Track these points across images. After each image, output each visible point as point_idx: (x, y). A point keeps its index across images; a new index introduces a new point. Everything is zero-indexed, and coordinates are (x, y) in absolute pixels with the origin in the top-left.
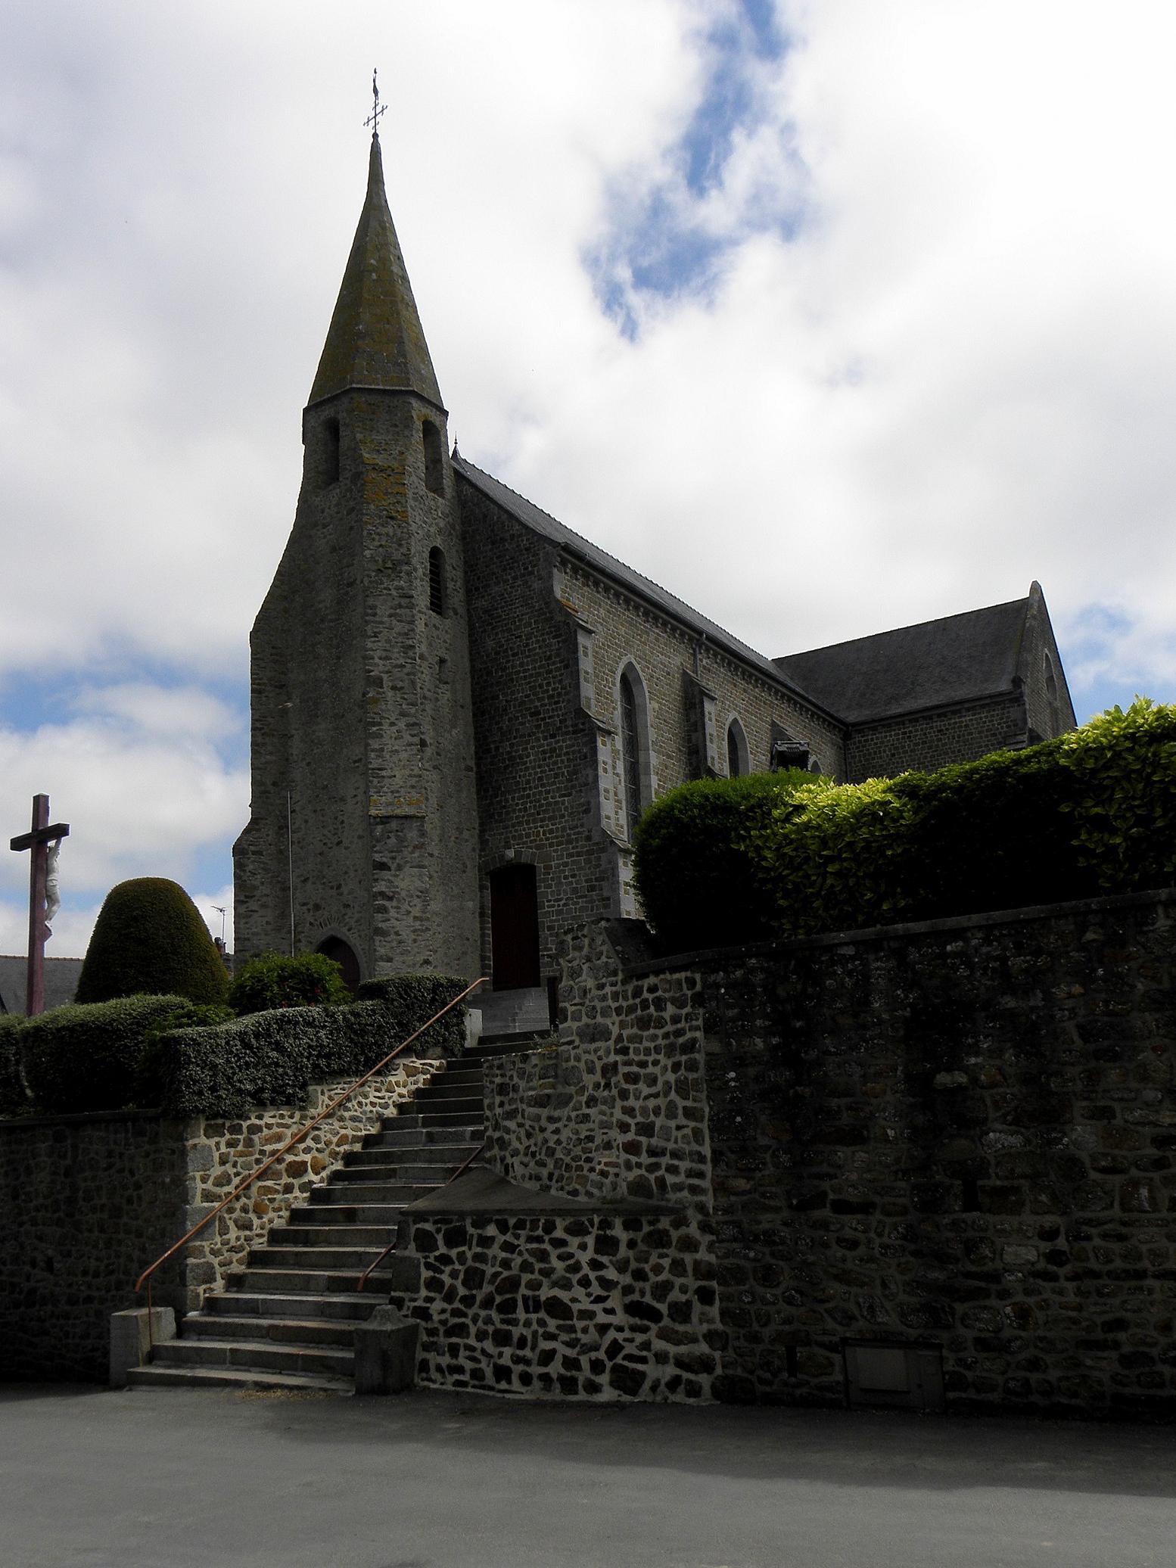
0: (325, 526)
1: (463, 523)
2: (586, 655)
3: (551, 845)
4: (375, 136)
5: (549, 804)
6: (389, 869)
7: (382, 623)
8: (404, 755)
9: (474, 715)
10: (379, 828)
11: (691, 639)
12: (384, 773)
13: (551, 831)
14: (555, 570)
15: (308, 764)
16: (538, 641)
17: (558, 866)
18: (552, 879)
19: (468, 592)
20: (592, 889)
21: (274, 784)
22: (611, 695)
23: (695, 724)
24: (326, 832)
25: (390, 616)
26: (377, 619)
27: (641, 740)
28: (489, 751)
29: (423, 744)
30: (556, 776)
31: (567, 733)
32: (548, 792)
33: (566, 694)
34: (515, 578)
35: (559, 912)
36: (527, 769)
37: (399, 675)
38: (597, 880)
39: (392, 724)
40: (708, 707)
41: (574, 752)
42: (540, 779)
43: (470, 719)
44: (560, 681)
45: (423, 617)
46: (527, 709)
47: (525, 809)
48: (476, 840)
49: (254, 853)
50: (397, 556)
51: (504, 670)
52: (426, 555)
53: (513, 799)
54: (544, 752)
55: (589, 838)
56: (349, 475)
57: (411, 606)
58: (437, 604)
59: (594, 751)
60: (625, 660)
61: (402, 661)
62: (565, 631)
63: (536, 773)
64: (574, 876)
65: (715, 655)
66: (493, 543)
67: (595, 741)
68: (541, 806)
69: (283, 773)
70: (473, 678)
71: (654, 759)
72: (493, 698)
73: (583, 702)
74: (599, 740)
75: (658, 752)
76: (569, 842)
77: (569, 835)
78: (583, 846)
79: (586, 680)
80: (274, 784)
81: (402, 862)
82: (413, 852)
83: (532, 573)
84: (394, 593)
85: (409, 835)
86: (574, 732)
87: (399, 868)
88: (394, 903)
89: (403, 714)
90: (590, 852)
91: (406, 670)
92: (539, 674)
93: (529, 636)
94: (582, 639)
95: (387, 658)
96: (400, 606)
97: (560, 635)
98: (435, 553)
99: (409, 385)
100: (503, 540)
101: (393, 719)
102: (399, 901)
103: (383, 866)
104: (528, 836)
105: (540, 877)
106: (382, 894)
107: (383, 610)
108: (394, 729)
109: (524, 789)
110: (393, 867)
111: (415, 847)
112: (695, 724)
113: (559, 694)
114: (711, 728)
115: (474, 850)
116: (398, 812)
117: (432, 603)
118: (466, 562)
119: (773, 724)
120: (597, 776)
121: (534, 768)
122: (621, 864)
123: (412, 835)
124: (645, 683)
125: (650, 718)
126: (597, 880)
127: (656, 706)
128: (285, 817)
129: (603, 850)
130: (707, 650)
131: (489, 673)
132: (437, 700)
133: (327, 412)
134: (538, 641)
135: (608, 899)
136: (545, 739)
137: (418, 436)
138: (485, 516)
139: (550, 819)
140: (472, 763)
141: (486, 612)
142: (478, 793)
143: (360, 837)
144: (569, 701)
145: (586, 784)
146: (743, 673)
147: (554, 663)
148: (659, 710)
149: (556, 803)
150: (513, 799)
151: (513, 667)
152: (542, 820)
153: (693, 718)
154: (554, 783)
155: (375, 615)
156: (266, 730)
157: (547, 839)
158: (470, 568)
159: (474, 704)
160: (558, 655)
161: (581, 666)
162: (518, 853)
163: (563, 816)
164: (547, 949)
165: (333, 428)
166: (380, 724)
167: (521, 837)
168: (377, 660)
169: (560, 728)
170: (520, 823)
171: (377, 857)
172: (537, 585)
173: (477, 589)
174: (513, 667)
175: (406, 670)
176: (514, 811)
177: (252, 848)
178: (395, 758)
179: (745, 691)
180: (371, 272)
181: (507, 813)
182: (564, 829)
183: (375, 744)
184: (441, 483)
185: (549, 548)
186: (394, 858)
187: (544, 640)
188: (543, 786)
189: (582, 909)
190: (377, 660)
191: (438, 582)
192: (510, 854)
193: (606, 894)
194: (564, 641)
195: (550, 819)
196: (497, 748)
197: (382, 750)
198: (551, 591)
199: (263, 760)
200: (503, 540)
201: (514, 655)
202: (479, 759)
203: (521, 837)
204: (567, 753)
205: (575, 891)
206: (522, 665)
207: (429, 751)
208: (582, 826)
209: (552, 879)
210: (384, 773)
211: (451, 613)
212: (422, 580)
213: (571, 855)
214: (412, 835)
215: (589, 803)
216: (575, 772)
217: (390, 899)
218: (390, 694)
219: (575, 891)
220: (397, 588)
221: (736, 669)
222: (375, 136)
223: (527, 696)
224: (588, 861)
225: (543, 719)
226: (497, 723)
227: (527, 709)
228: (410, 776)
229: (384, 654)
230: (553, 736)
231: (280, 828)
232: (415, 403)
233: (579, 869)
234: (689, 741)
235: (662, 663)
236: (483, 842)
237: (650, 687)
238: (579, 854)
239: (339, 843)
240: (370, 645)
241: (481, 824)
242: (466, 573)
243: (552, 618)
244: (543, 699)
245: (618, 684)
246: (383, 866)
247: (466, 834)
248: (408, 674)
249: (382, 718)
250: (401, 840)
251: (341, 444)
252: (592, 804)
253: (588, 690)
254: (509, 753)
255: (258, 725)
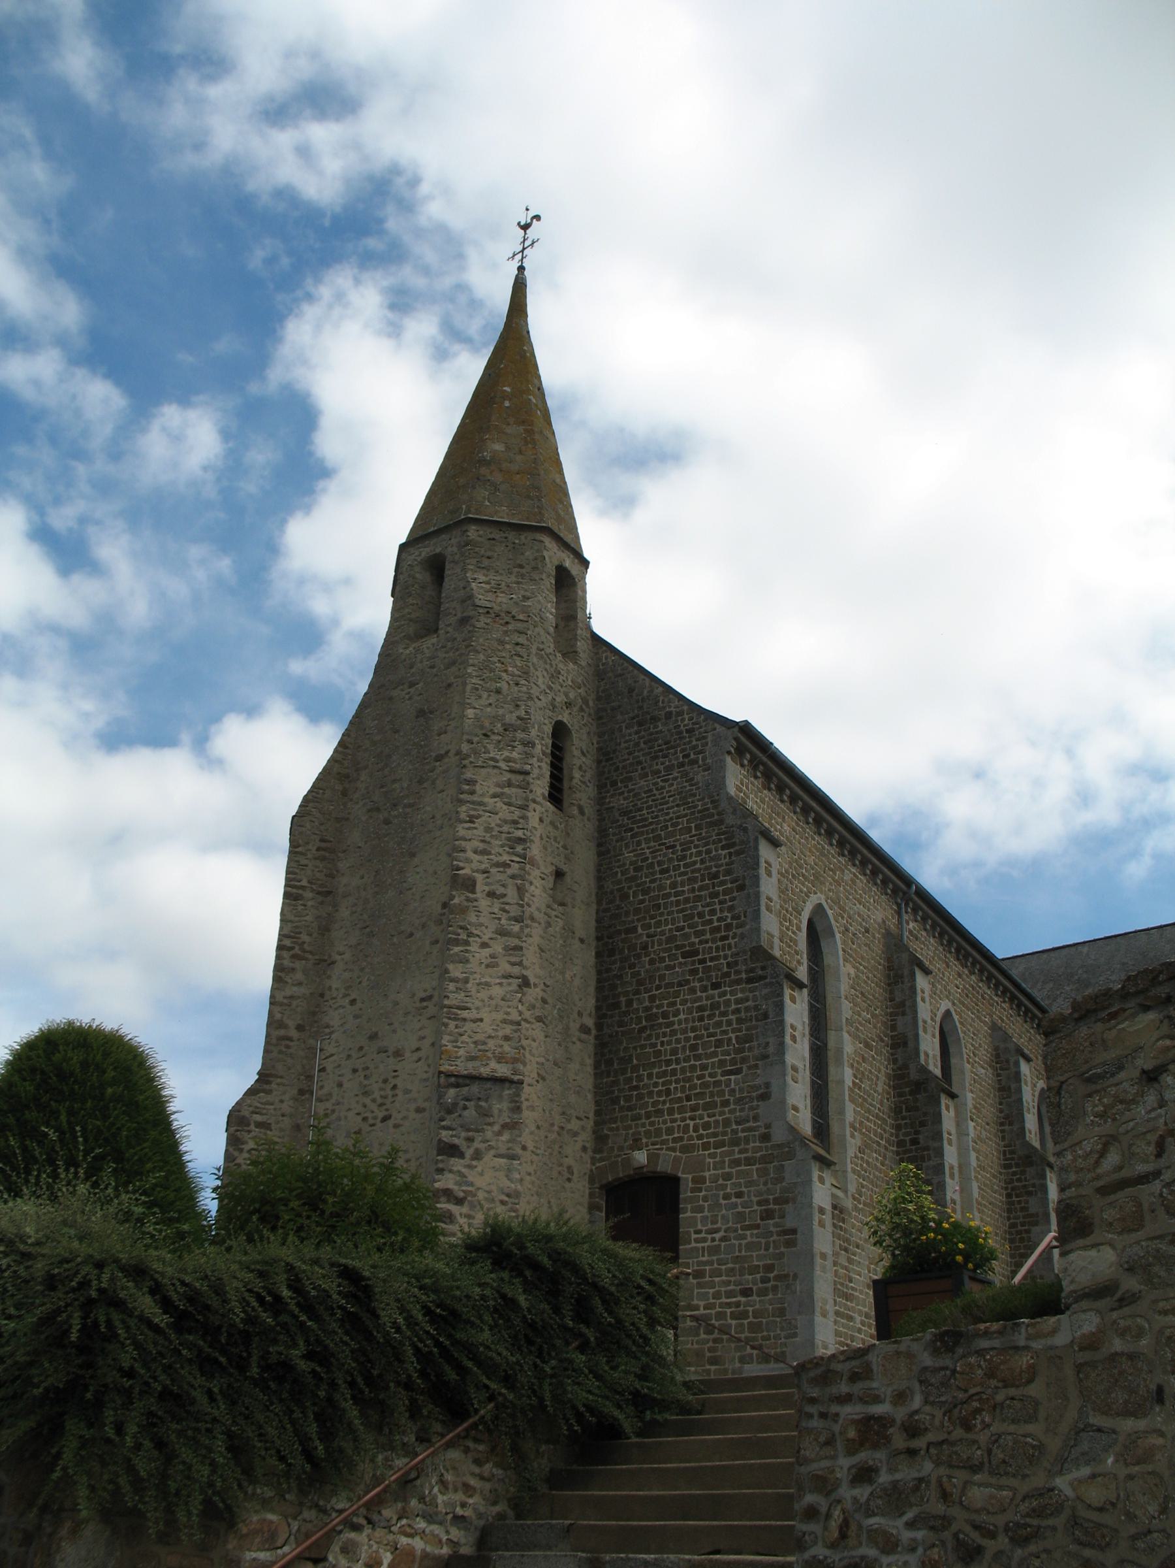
0: (412, 685)
1: (598, 698)
2: (769, 874)
3: (706, 1146)
4: (521, 269)
5: (705, 1085)
6: (462, 1155)
7: (481, 804)
8: (497, 991)
9: (598, 955)
10: (452, 1092)
11: (895, 891)
12: (464, 1014)
13: (706, 1126)
14: (728, 759)
15: (353, 1002)
16: (699, 853)
17: (715, 1179)
18: (705, 1199)
19: (601, 787)
20: (768, 1215)
21: (300, 1028)
22: (796, 942)
23: (902, 1004)
24: (367, 1101)
25: (494, 796)
26: (475, 798)
27: (831, 1015)
28: (616, 1005)
29: (525, 983)
30: (719, 1044)
31: (738, 982)
32: (704, 1067)
33: (739, 926)
34: (669, 769)
35: (714, 1250)
36: (674, 1033)
37: (499, 877)
38: (776, 1201)
39: (484, 945)
40: (922, 982)
41: (747, 1009)
42: (694, 1048)
43: (592, 960)
44: (731, 909)
45: (538, 808)
46: (677, 947)
47: (668, 1092)
48: (586, 1137)
49: (259, 1125)
50: (511, 718)
51: (646, 892)
52: (548, 729)
53: (650, 1076)
54: (701, 1009)
55: (766, 1137)
56: (452, 620)
57: (525, 786)
58: (556, 796)
59: (780, 1007)
60: (814, 900)
61: (506, 858)
62: (741, 839)
63: (687, 1039)
64: (739, 1195)
65: (924, 919)
66: (640, 724)
67: (781, 995)
68: (693, 1087)
69: (314, 1014)
70: (599, 902)
71: (849, 1047)
72: (628, 931)
73: (764, 936)
74: (787, 992)
75: (855, 1037)
76: (735, 1142)
77: (735, 1132)
78: (755, 1150)
79: (769, 909)
80: (300, 1028)
81: (482, 1146)
82: (499, 1133)
83: (695, 762)
84: (503, 765)
85: (496, 1106)
86: (750, 981)
87: (477, 1156)
88: (465, 1209)
89: (502, 933)
90: (765, 1160)
91: (509, 871)
92: (698, 898)
93: (686, 846)
94: (765, 851)
95: (484, 852)
96: (509, 784)
97: (734, 844)
98: (560, 732)
99: (541, 521)
100: (654, 719)
101: (485, 938)
102: (472, 1206)
103: (452, 1150)
104: (670, 1131)
105: (685, 1194)
106: (447, 1193)
107: (487, 785)
108: (486, 952)
109: (668, 1062)
110: (469, 1153)
111: (505, 1126)
112: (902, 1004)
113: (728, 927)
114: (924, 1011)
115: (584, 1149)
116: (484, 1071)
117: (550, 794)
118: (599, 749)
119: (994, 1027)
120: (782, 1044)
121: (684, 1031)
122: (815, 1178)
123: (500, 1107)
124: (838, 936)
125: (844, 987)
126: (776, 1201)
127: (852, 971)
128: (310, 1078)
129: (791, 1155)
130: (915, 910)
131: (625, 897)
132: (549, 925)
133: (425, 551)
134: (699, 853)
135: (794, 1231)
136: (704, 989)
137: (549, 582)
138: (631, 690)
139: (707, 1107)
140: (590, 1022)
141: (625, 813)
142: (597, 1065)
143: (419, 1110)
144: (742, 936)
145: (765, 1057)
146: (958, 951)
147: (723, 883)
148: (851, 974)
149: (717, 1084)
150: (650, 1076)
151: (661, 888)
152: (694, 1109)
153: (899, 997)
154: (715, 1054)
155: (472, 793)
156: (297, 950)
157: (700, 1137)
158: (605, 756)
159: (598, 939)
160: (728, 872)
161: (762, 889)
162: (653, 1157)
163: (726, 1103)
164: (690, 1307)
165: (437, 568)
166: (467, 943)
167: (658, 1133)
168: (470, 854)
169: (727, 975)
170: (659, 1113)
171: (445, 1135)
172: (700, 777)
173: (614, 783)
174: (661, 888)
175: (509, 871)
176: (650, 1094)
177: (258, 1118)
178: (483, 995)
179: (959, 975)
180: (504, 399)
181: (640, 1097)
182: (727, 1123)
183: (456, 971)
184: (574, 646)
185: (720, 729)
186: (470, 1140)
187: (708, 852)
188: (698, 1057)
189: (749, 1247)
190: (470, 854)
191: (560, 770)
192: (641, 1157)
193: (789, 1223)
194: (738, 853)
195: (707, 1107)
196: (629, 1003)
197: (466, 981)
198: (722, 784)
199: (288, 993)
200: (654, 719)
201: (662, 872)
202: (601, 1014)
203: (658, 1133)
204: (737, 1011)
205: (740, 1217)
206: (674, 885)
207: (533, 994)
208: (756, 1118)
209: (705, 1199)
210: (464, 1014)
211: (576, 812)
212: (540, 760)
213: (737, 1163)
214: (500, 1107)
215: (767, 1085)
216: (748, 1039)
217: (459, 1202)
218: (484, 903)
219: (740, 1217)
220: (508, 760)
221: (950, 942)
222: (521, 269)
223: (679, 929)
224: (763, 1172)
225: (702, 961)
226: (632, 966)
227: (677, 947)
228: (505, 1021)
229: (481, 846)
230: (716, 986)
231: (301, 1092)
232: (548, 541)
233: (750, 1184)
234: (893, 1028)
235: (866, 911)
236: (600, 1139)
237: (844, 942)
238: (749, 1162)
239: (385, 1119)
240: (462, 832)
241: (598, 1113)
242: (599, 762)
243: (721, 822)
244: (703, 933)
245: (804, 930)
246: (452, 1150)
247: (574, 1125)
248: (513, 877)
249: (470, 935)
250: (485, 1114)
251: (446, 584)
252: (774, 1089)
253: (770, 924)
254: (647, 1009)
255: (287, 942)
